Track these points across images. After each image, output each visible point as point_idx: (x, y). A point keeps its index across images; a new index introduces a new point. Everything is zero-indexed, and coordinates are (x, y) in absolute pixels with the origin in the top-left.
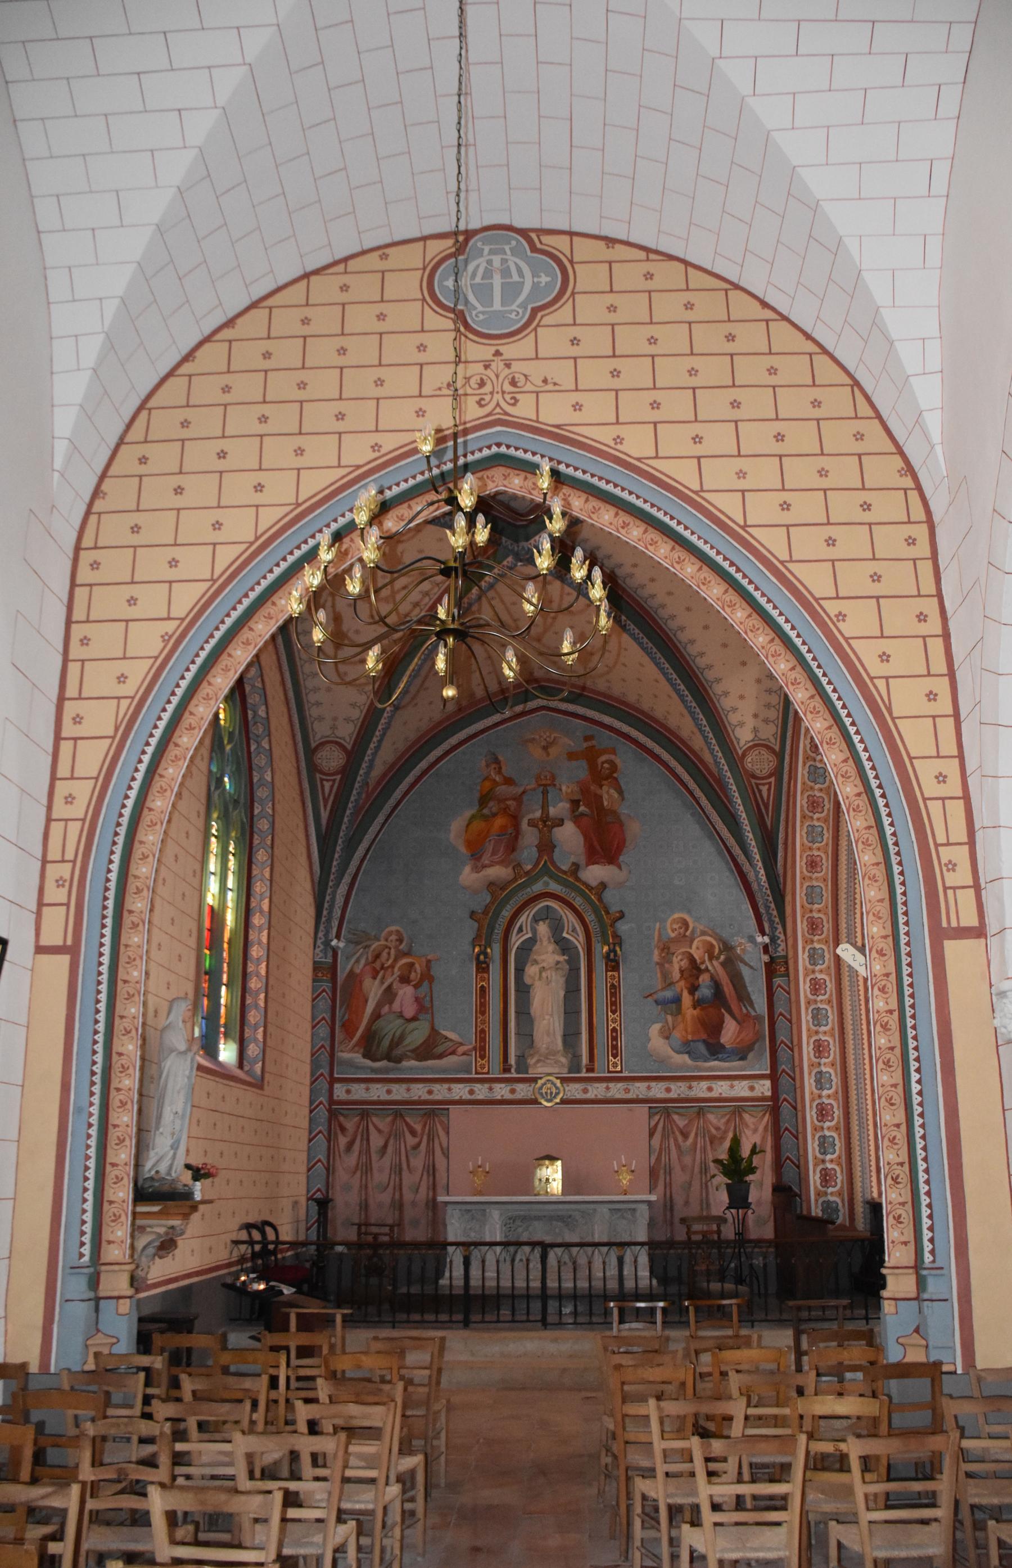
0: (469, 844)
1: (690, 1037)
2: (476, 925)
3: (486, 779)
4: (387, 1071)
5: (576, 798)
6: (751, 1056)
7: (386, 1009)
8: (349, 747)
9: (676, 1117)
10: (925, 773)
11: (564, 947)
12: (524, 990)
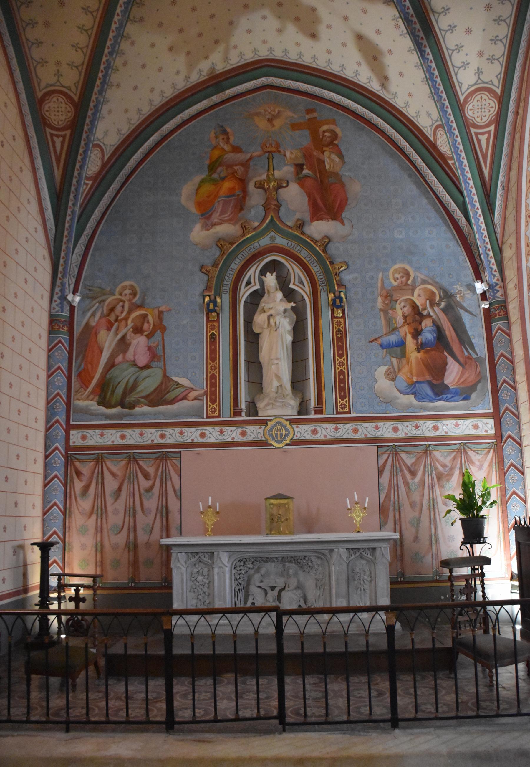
0: (199, 205)
1: (415, 379)
2: (206, 278)
3: (215, 148)
4: (120, 416)
5: (300, 162)
6: (473, 396)
7: (120, 358)
8: (76, 98)
9: (403, 456)
11: (289, 295)
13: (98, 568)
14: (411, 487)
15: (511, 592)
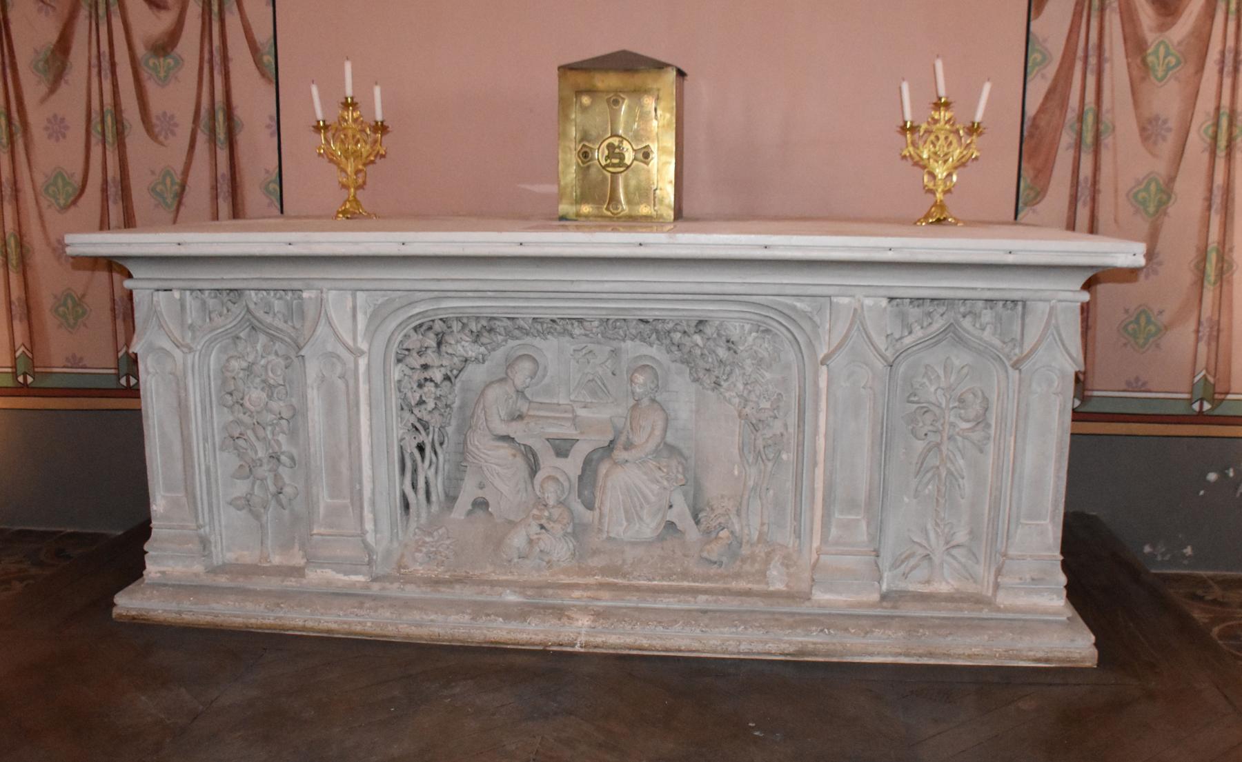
13: (16, 323)
14: (1150, 59)
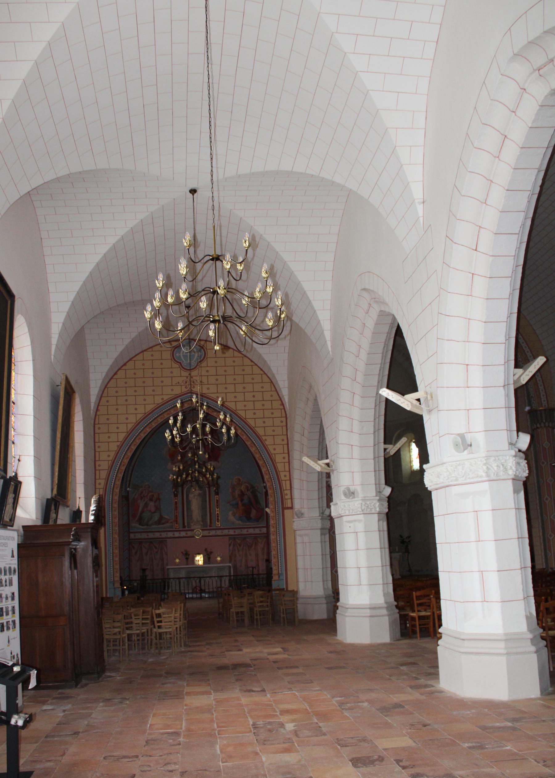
9: (237, 540)
10: (282, 475)
12: (189, 502)
15: (3, 649)
